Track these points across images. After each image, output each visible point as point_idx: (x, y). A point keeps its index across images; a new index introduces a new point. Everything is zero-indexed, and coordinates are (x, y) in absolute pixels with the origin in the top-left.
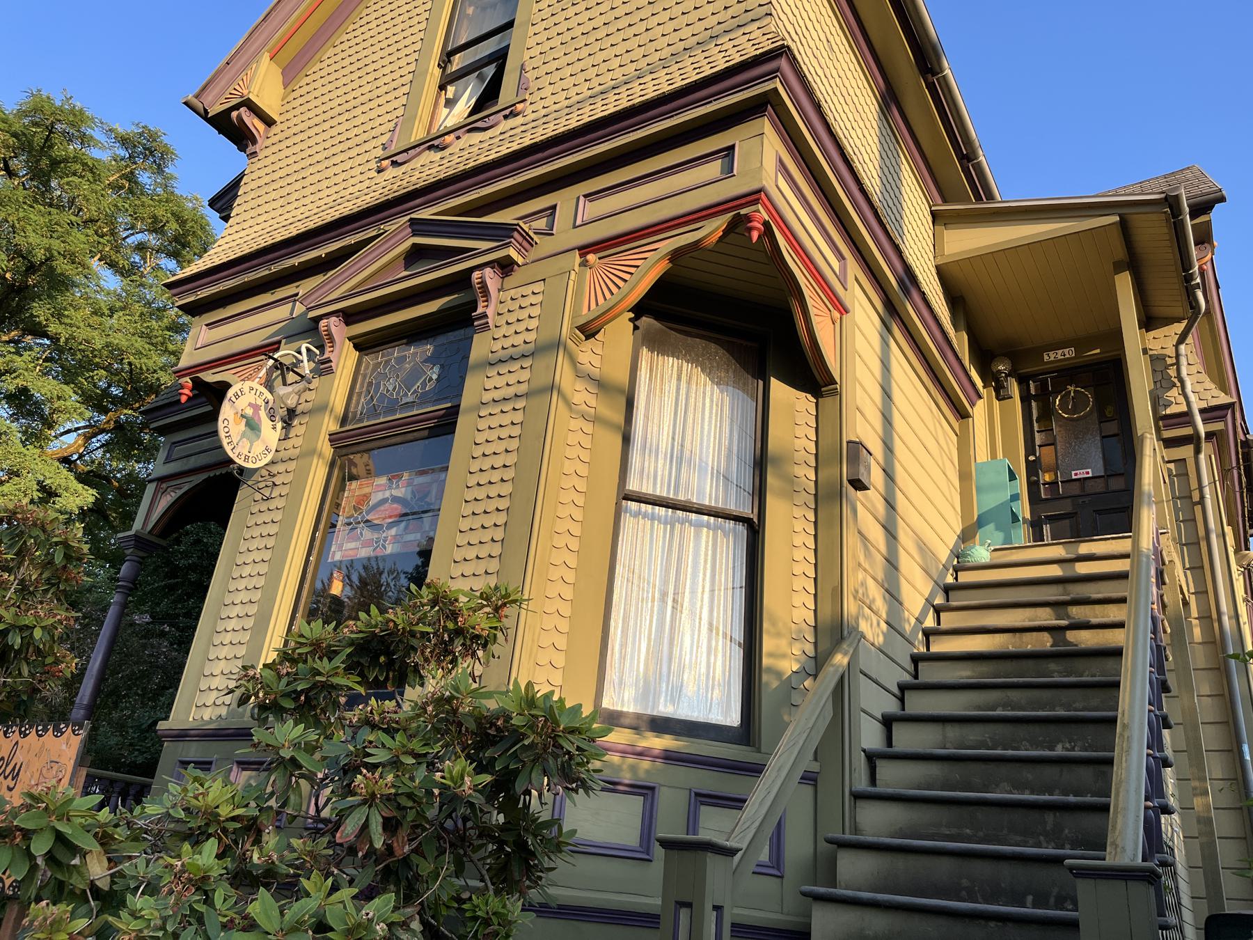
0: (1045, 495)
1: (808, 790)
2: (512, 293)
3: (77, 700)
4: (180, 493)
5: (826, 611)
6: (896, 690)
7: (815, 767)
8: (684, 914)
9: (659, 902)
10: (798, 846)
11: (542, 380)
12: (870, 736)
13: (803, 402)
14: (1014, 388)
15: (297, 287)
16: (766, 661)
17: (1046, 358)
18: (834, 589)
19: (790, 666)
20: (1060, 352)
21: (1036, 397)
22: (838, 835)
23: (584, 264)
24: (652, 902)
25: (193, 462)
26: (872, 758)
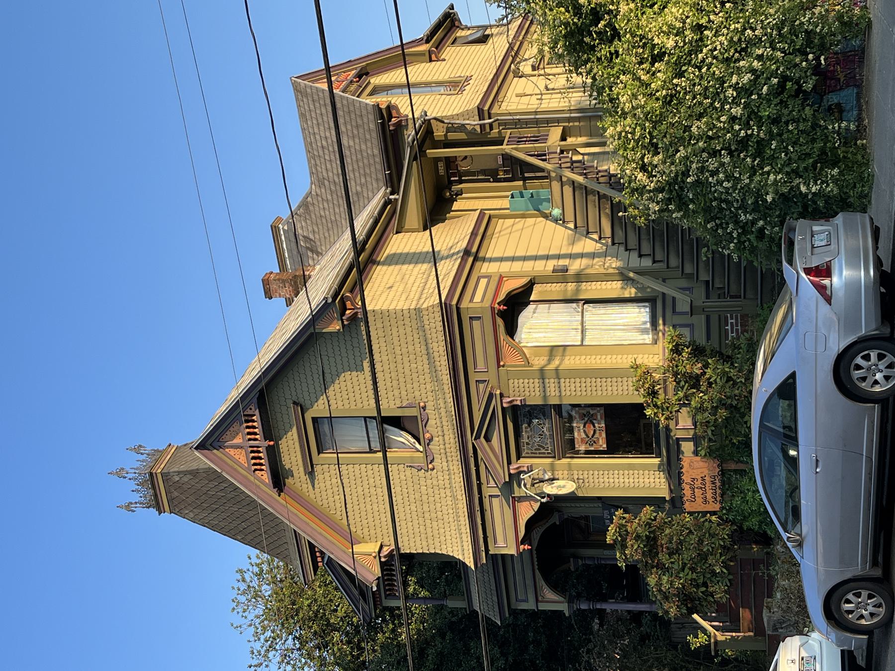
0: (509, 175)
1: (667, 281)
2: (511, 392)
3: (649, 610)
4: (545, 586)
5: (617, 278)
6: (628, 252)
7: (661, 279)
8: (705, 310)
9: (703, 316)
10: (683, 283)
11: (553, 374)
12: (647, 263)
13: (537, 289)
14: (455, 188)
15: (485, 497)
16: (633, 296)
17: (442, 174)
18: (605, 276)
19: (633, 291)
20: (440, 168)
21: (460, 177)
22: (681, 273)
23: (503, 366)
24: (703, 317)
25: (530, 582)
26: (654, 262)
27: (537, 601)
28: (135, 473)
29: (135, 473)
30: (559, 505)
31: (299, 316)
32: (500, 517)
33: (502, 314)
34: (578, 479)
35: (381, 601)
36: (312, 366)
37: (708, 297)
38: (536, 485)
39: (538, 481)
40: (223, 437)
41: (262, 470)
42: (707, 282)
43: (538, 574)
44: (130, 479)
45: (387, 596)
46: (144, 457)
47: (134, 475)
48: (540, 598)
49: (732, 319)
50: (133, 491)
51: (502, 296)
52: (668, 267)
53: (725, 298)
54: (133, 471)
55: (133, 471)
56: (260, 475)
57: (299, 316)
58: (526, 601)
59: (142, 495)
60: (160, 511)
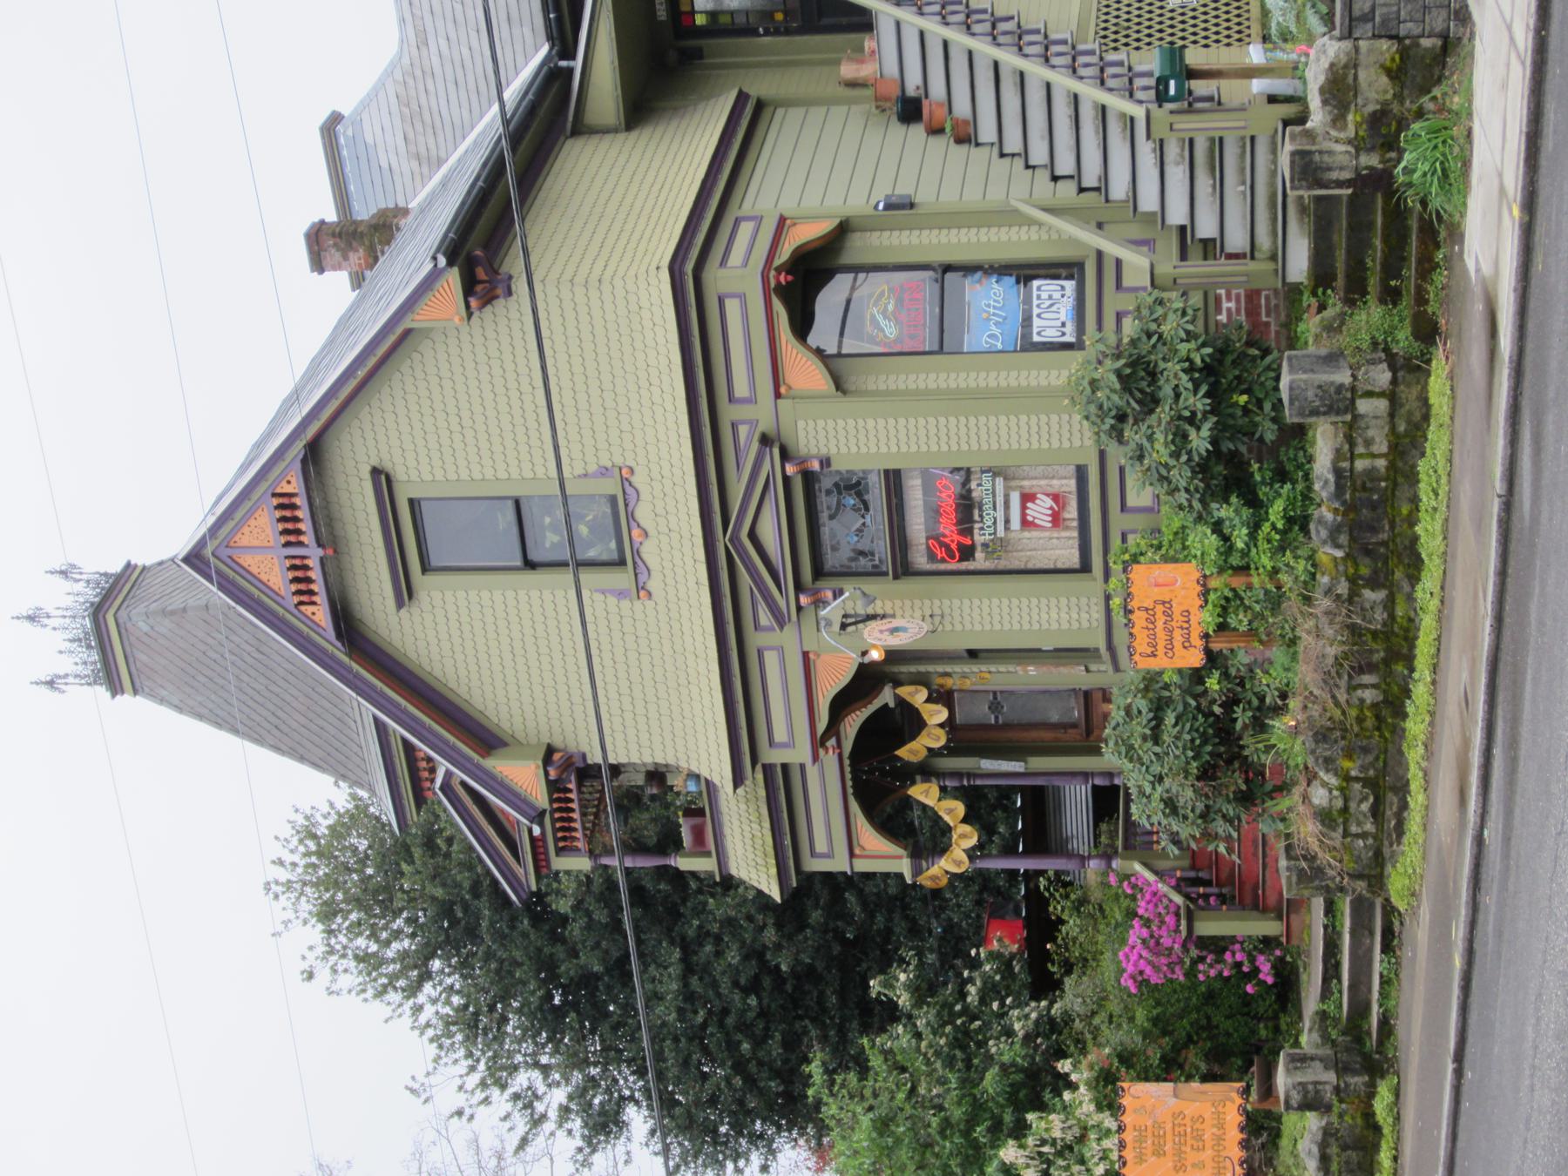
1: (1106, 227)
10: (1135, 231)
27: (852, 855)
28: (65, 617)
29: (65, 617)
30: (896, 669)
31: (381, 298)
32: (1516, 147)
33: (784, 293)
34: (931, 616)
35: (547, 860)
36: (407, 397)
37: (1183, 256)
38: (850, 629)
39: (853, 620)
40: (237, 539)
41: (314, 603)
42: (1182, 229)
43: (855, 807)
44: (54, 629)
45: (560, 851)
46: (80, 587)
47: (62, 621)
48: (857, 851)
49: (1229, 299)
50: (61, 652)
51: (784, 254)
52: (1107, 201)
53: (1215, 259)
54: (60, 612)
55: (60, 612)
56: (309, 613)
57: (381, 298)
58: (829, 855)
59: (78, 660)
60: (115, 688)
